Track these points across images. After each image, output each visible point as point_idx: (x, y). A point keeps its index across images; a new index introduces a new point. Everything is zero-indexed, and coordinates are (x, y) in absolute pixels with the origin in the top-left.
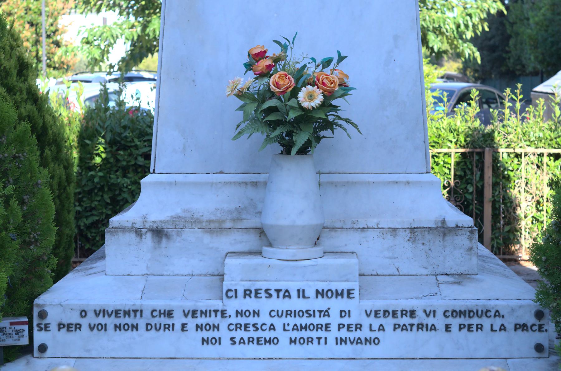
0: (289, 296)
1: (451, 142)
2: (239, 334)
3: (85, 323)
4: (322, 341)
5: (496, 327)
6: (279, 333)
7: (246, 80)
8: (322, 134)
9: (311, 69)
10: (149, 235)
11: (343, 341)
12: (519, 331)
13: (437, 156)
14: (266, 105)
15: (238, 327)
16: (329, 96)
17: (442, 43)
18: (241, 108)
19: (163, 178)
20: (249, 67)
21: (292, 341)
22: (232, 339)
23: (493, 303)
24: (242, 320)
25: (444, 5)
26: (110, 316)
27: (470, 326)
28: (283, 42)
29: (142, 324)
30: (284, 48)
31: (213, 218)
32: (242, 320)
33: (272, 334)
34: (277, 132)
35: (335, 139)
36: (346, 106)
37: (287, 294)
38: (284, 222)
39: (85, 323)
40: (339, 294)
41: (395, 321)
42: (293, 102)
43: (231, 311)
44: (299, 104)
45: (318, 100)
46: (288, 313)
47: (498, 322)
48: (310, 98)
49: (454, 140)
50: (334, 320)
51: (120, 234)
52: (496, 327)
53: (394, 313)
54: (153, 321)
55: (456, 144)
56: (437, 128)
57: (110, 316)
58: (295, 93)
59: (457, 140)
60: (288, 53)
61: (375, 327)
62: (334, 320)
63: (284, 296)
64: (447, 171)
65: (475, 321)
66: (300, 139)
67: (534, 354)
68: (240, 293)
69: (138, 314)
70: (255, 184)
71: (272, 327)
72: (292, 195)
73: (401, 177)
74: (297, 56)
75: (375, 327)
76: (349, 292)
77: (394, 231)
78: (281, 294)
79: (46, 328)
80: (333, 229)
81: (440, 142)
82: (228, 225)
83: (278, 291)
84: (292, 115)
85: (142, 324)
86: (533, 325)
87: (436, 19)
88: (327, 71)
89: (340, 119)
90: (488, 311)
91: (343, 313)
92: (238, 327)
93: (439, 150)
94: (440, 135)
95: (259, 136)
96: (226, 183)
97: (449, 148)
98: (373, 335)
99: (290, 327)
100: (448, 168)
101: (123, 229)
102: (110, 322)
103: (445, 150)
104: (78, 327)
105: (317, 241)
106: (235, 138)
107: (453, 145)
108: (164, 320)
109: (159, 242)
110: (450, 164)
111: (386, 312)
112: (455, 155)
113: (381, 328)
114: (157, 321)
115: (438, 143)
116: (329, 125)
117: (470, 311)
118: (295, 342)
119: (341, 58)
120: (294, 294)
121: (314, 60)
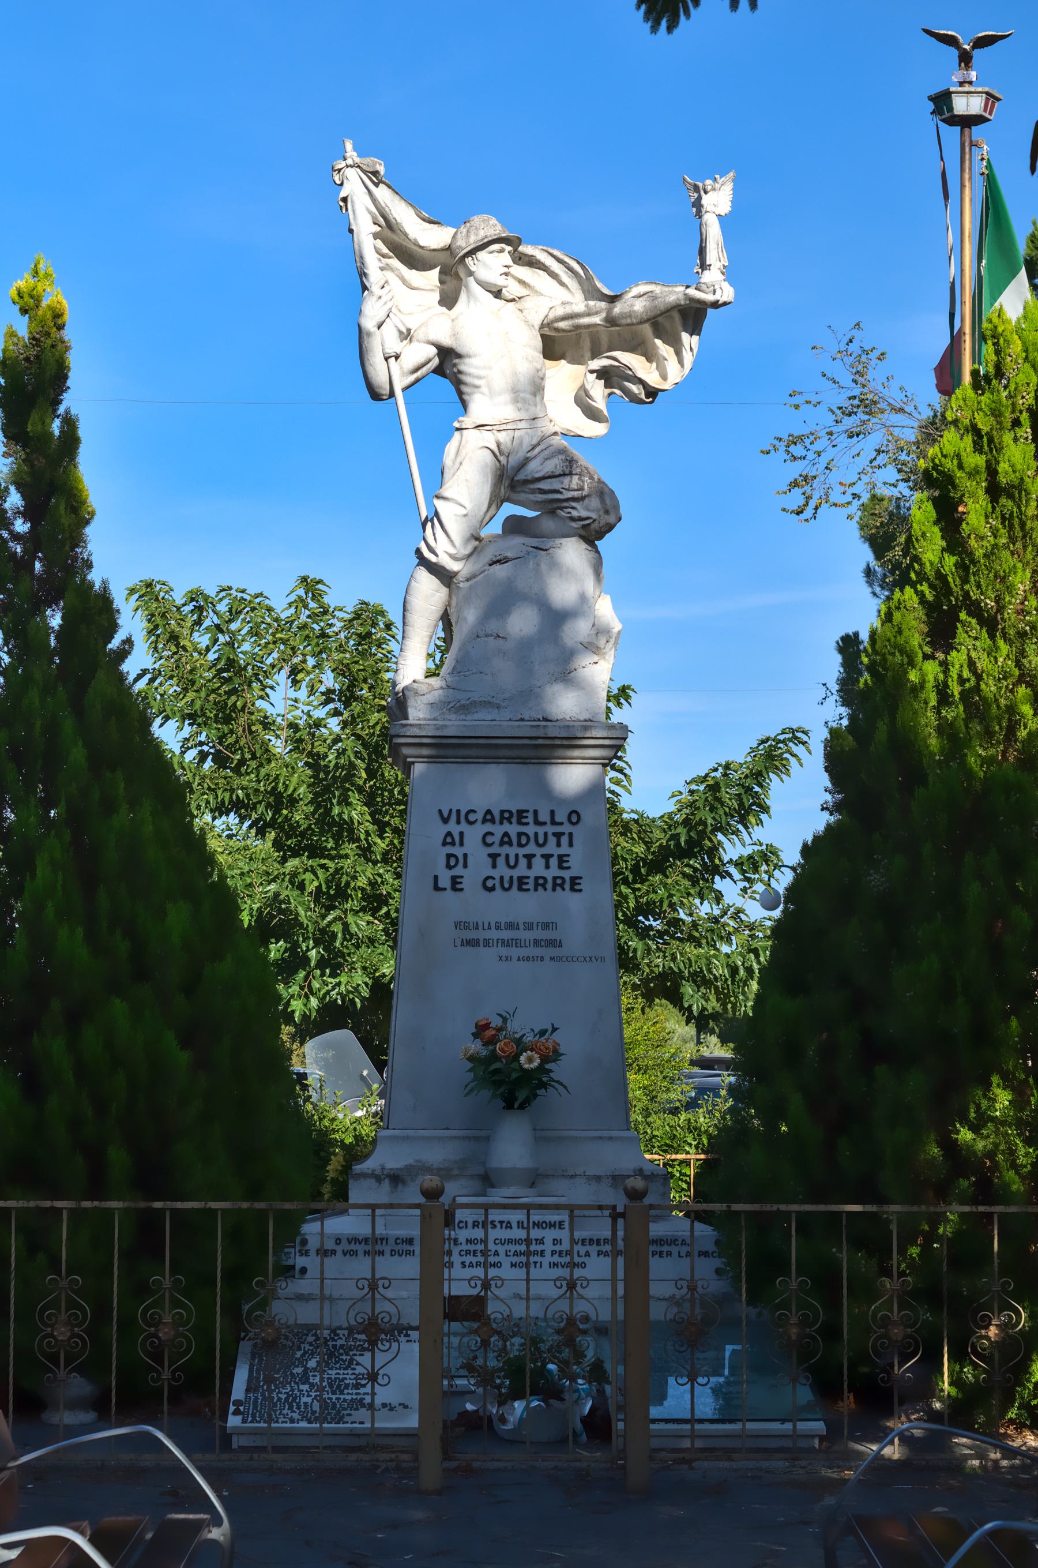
0: (511, 1227)
1: (690, 1145)
2: (468, 1259)
3: (339, 1249)
4: (538, 1265)
5: (683, 1254)
6: (502, 1258)
7: (476, 1047)
8: (538, 1092)
9: (529, 1038)
10: (387, 1181)
11: (555, 1265)
12: (702, 1257)
13: (671, 1166)
14: (492, 1068)
15: (468, 1252)
16: (545, 1059)
17: (707, 1000)
18: (470, 1070)
19: (396, 1132)
20: (476, 1036)
21: (513, 1265)
22: (463, 1263)
23: (680, 1234)
24: (472, 1247)
25: (712, 931)
26: (360, 1243)
27: (661, 1253)
28: (504, 1014)
29: (388, 1250)
30: (505, 1020)
31: (441, 1166)
32: (472, 1247)
33: (496, 1259)
34: (502, 1090)
35: (548, 1097)
36: (559, 1070)
37: (509, 1226)
38: (505, 1165)
39: (339, 1249)
40: (552, 1225)
41: (599, 1248)
42: (514, 1065)
43: (462, 1239)
44: (520, 1066)
45: (536, 1063)
46: (510, 1241)
47: (684, 1250)
48: (529, 1061)
49: (694, 1143)
50: (548, 1247)
51: (362, 1180)
52: (683, 1254)
53: (598, 1242)
54: (397, 1248)
55: (697, 1147)
56: (671, 1127)
57: (360, 1243)
58: (516, 1057)
59: (699, 1143)
60: (508, 1025)
61: (582, 1253)
62: (548, 1247)
63: (507, 1227)
64: (684, 1186)
65: (665, 1248)
66: (522, 1095)
67: (716, 1277)
68: (470, 1225)
69: (384, 1242)
70: (477, 1139)
71: (496, 1253)
72: (512, 1146)
73: (605, 1134)
74: (517, 1027)
75: (582, 1253)
76: (561, 1223)
77: (598, 1178)
78: (504, 1225)
79: (307, 1253)
80: (547, 1176)
81: (675, 1145)
82: (455, 1172)
83: (501, 1222)
84: (514, 1075)
85: (388, 1250)
86: (714, 1252)
87: (693, 959)
88: (543, 1039)
89: (554, 1081)
90: (676, 1240)
91: (555, 1242)
92: (468, 1252)
93: (674, 1157)
94: (675, 1136)
95: (486, 1094)
96: (455, 1137)
97: (688, 1153)
98: (580, 1260)
99: (512, 1253)
100: (686, 1182)
101: (364, 1175)
102: (361, 1248)
103: (681, 1156)
104: (334, 1252)
105: (532, 1185)
106: (466, 1095)
107: (693, 1151)
108: (406, 1247)
109: (396, 1187)
110: (689, 1176)
111: (591, 1240)
112: (695, 1164)
113: (587, 1254)
114: (399, 1247)
115: (672, 1147)
116: (544, 1085)
117: (661, 1240)
118: (515, 1266)
119: (554, 1029)
120: (514, 1225)
121: (532, 1030)
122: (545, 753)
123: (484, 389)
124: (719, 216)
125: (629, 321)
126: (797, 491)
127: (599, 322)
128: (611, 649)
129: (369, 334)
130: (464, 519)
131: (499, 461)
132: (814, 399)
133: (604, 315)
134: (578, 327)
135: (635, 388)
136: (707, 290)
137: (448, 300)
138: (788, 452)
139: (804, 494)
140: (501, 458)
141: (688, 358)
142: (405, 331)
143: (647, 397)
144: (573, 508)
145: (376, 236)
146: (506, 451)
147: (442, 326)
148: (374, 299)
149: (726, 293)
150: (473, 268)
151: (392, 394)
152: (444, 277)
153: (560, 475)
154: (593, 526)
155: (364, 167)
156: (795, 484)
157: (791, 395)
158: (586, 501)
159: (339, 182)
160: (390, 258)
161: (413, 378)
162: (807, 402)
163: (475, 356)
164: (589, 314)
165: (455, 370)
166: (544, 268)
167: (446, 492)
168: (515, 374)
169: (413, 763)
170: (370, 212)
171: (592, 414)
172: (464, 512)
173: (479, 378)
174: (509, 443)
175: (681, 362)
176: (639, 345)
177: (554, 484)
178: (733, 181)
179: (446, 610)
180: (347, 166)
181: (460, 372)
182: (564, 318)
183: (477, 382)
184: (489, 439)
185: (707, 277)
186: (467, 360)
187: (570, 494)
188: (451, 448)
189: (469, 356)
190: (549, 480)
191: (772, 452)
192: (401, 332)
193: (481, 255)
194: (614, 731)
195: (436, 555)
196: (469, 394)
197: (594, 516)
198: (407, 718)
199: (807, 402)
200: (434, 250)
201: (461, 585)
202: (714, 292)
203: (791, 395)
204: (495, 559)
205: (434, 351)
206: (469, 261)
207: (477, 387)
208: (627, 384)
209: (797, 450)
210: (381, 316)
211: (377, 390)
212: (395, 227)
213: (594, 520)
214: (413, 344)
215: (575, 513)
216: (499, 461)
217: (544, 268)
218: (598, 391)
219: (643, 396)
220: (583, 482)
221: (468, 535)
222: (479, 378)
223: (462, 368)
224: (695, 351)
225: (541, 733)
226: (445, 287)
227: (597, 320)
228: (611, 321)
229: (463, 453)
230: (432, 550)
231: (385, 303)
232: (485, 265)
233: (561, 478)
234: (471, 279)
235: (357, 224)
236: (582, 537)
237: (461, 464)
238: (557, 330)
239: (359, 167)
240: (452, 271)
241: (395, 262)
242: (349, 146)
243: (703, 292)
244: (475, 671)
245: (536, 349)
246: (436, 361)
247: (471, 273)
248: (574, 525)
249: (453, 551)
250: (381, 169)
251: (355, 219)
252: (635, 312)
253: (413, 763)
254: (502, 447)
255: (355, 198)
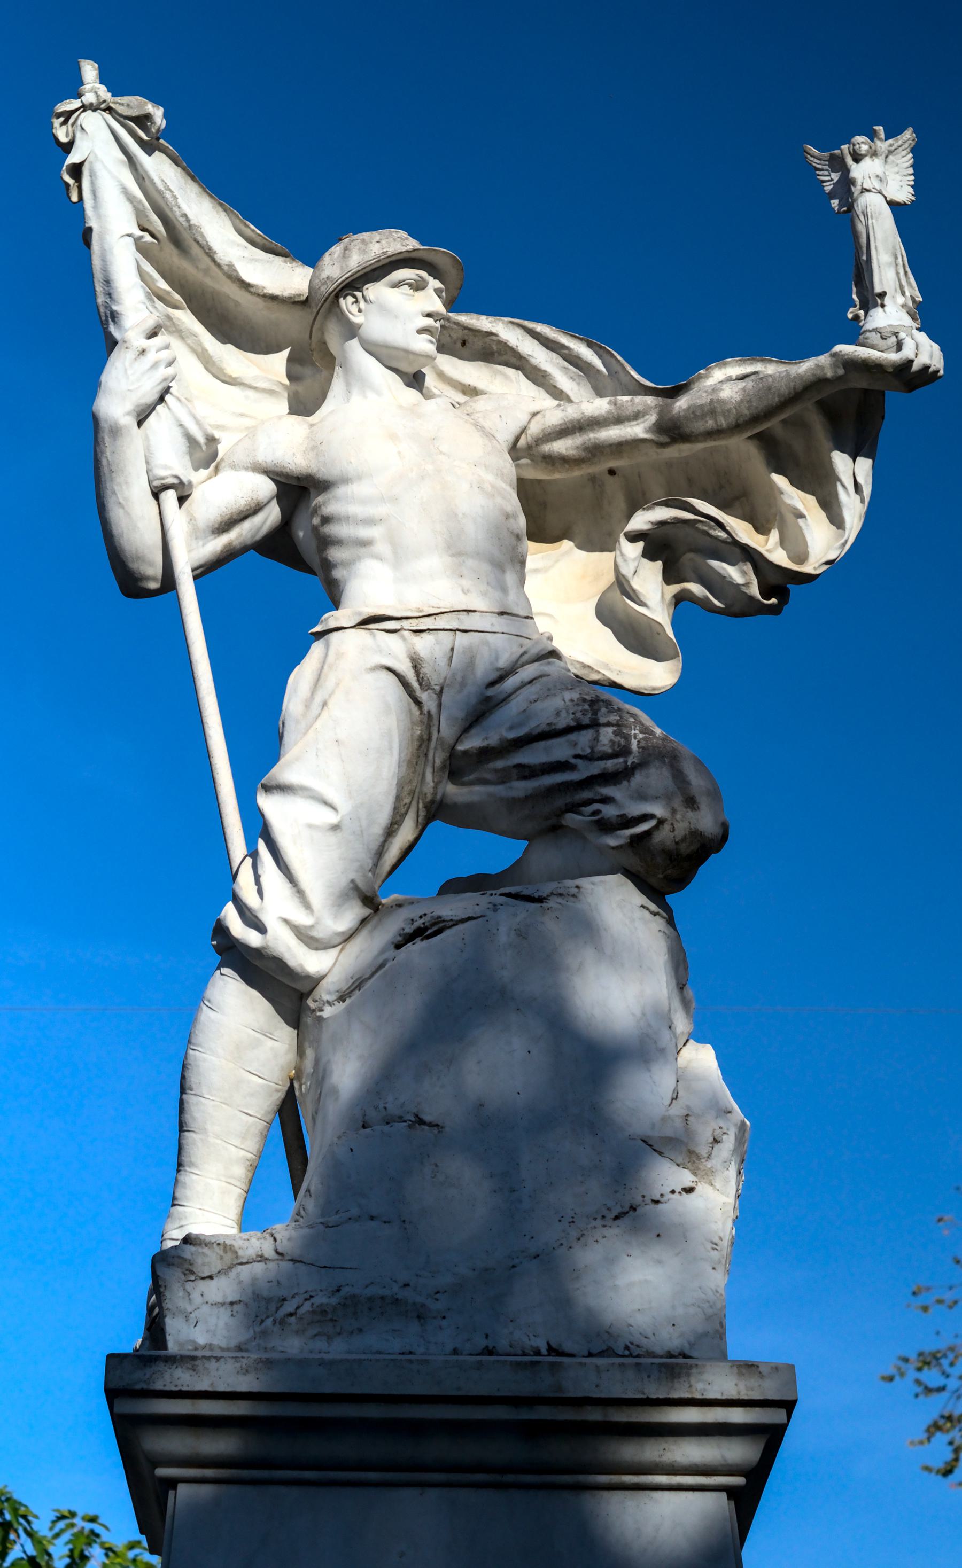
122: (559, 1450)
123: (381, 547)
124: (891, 204)
125: (710, 424)
126: (941, 1439)
127: (643, 435)
128: (727, 1162)
129: (116, 431)
130: (333, 838)
131: (418, 703)
132: (948, 1296)
133: (652, 418)
134: (595, 451)
135: (735, 573)
136: (882, 344)
137: (303, 405)
138: (918, 1382)
139: (951, 1443)
140: (424, 696)
141: (854, 510)
142: (201, 439)
143: (766, 594)
144: (606, 800)
145: (141, 248)
146: (435, 680)
147: (289, 442)
148: (130, 355)
149: (925, 352)
150: (357, 319)
151: (169, 582)
152: (298, 369)
153: (568, 730)
154: (658, 838)
155: (120, 109)
156: (935, 1428)
157: (914, 1293)
158: (638, 778)
159: (63, 139)
160: (176, 307)
161: (216, 545)
162: (940, 1302)
163: (359, 478)
164: (618, 420)
165: (316, 521)
166: (517, 361)
167: (288, 770)
168: (452, 515)
169: (172, 1483)
170: (130, 198)
171: (637, 637)
172: (333, 818)
173: (370, 522)
174: (443, 662)
175: (836, 520)
176: (737, 498)
177: (559, 750)
178: (912, 151)
179: (291, 1090)
180: (84, 108)
181: (326, 520)
182: (564, 431)
183: (364, 532)
184: (395, 650)
185: (879, 319)
186: (341, 491)
187: (596, 768)
188: (300, 680)
189: (346, 480)
190: (542, 744)
191: (897, 1378)
192: (191, 441)
193: (373, 290)
194: (754, 1382)
195: (261, 928)
196: (347, 564)
197: (658, 810)
198: (165, 1347)
199: (940, 1302)
200: (273, 298)
201: (328, 1012)
202: (899, 346)
203: (914, 1293)
204: (409, 929)
205: (266, 487)
206: (347, 304)
207: (365, 543)
208: (715, 564)
209: (932, 1377)
210: (147, 390)
211: (134, 566)
212: (186, 235)
213: (661, 822)
214: (221, 475)
215: (609, 811)
216: (418, 703)
217: (517, 361)
218: (653, 593)
219: (755, 591)
220: (627, 738)
221: (344, 881)
222: (370, 522)
223: (328, 510)
224: (867, 491)
225: (543, 1385)
226: (300, 388)
227: (638, 430)
228: (671, 431)
229: (330, 680)
230: (252, 920)
231: (155, 365)
232: (384, 310)
233: (573, 737)
234: (354, 344)
235: (99, 216)
236: (630, 875)
237: (325, 704)
238: (551, 460)
239: (109, 110)
240: (309, 343)
241: (186, 318)
242: (89, 71)
243: (872, 347)
244: (355, 1211)
245: (501, 475)
246: (272, 515)
247: (352, 331)
248: (612, 841)
249: (302, 918)
250: (158, 114)
251: (96, 207)
252: (722, 402)
253: (172, 1483)
254: (426, 670)
255: (98, 167)
